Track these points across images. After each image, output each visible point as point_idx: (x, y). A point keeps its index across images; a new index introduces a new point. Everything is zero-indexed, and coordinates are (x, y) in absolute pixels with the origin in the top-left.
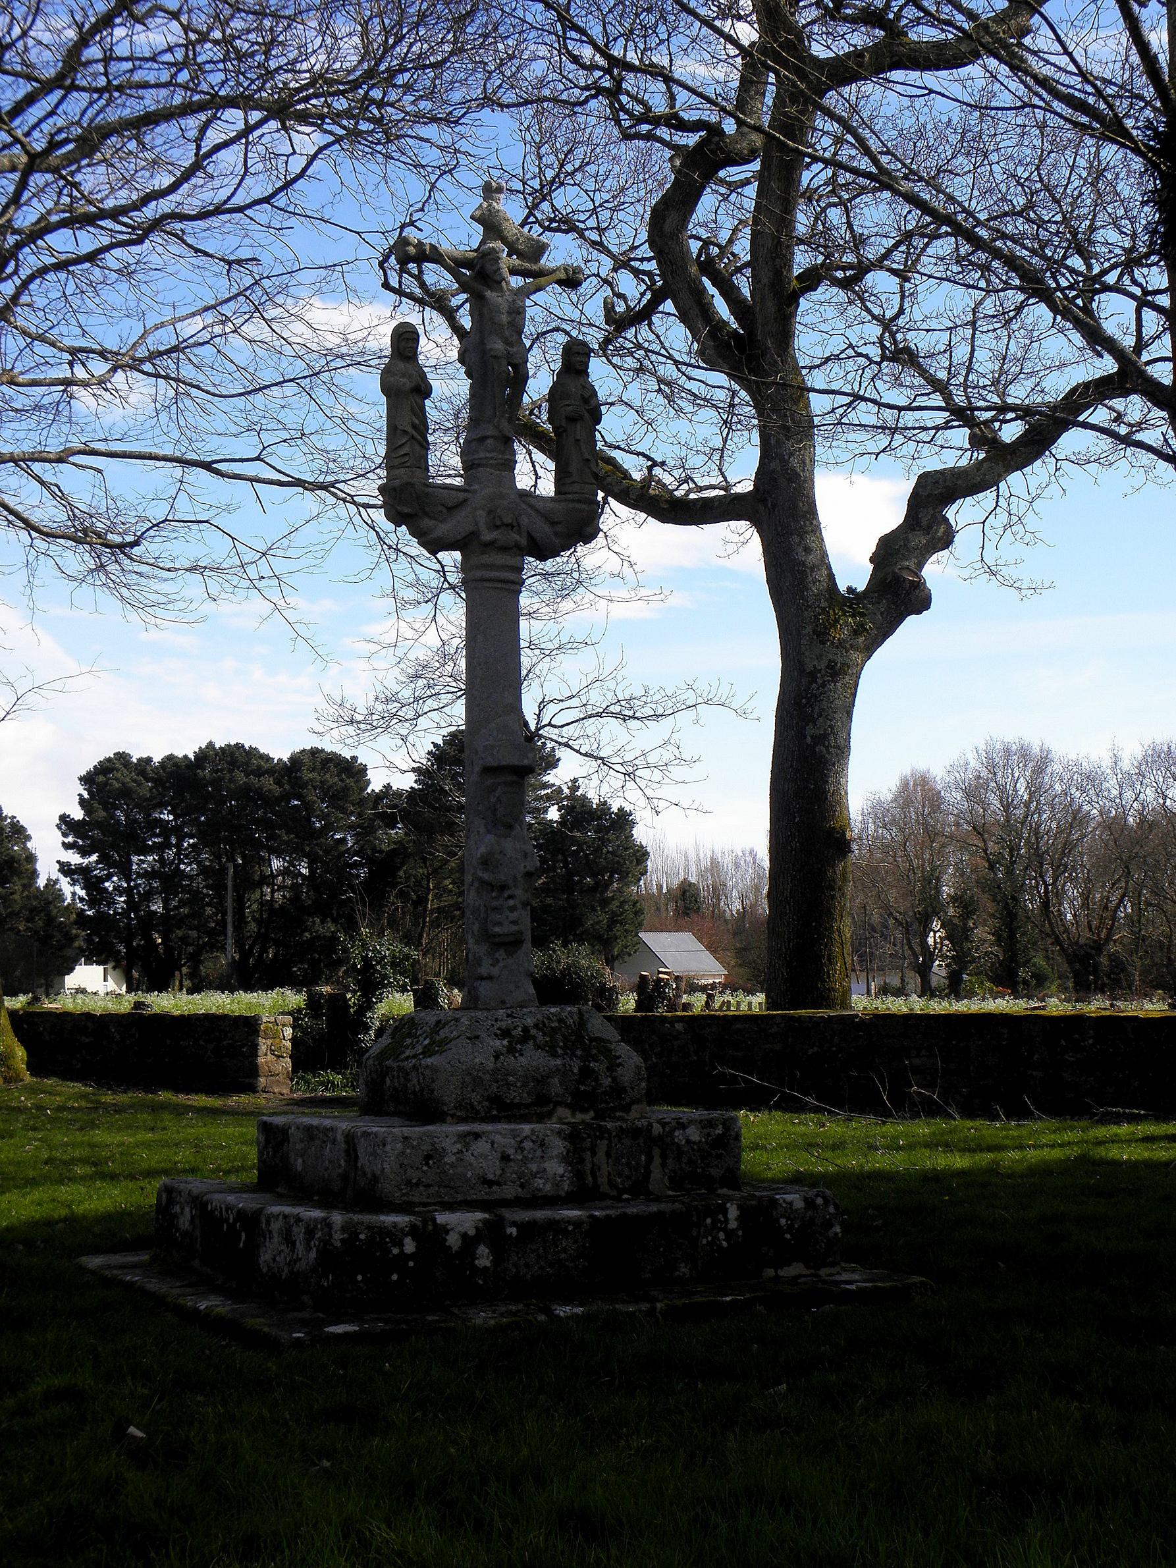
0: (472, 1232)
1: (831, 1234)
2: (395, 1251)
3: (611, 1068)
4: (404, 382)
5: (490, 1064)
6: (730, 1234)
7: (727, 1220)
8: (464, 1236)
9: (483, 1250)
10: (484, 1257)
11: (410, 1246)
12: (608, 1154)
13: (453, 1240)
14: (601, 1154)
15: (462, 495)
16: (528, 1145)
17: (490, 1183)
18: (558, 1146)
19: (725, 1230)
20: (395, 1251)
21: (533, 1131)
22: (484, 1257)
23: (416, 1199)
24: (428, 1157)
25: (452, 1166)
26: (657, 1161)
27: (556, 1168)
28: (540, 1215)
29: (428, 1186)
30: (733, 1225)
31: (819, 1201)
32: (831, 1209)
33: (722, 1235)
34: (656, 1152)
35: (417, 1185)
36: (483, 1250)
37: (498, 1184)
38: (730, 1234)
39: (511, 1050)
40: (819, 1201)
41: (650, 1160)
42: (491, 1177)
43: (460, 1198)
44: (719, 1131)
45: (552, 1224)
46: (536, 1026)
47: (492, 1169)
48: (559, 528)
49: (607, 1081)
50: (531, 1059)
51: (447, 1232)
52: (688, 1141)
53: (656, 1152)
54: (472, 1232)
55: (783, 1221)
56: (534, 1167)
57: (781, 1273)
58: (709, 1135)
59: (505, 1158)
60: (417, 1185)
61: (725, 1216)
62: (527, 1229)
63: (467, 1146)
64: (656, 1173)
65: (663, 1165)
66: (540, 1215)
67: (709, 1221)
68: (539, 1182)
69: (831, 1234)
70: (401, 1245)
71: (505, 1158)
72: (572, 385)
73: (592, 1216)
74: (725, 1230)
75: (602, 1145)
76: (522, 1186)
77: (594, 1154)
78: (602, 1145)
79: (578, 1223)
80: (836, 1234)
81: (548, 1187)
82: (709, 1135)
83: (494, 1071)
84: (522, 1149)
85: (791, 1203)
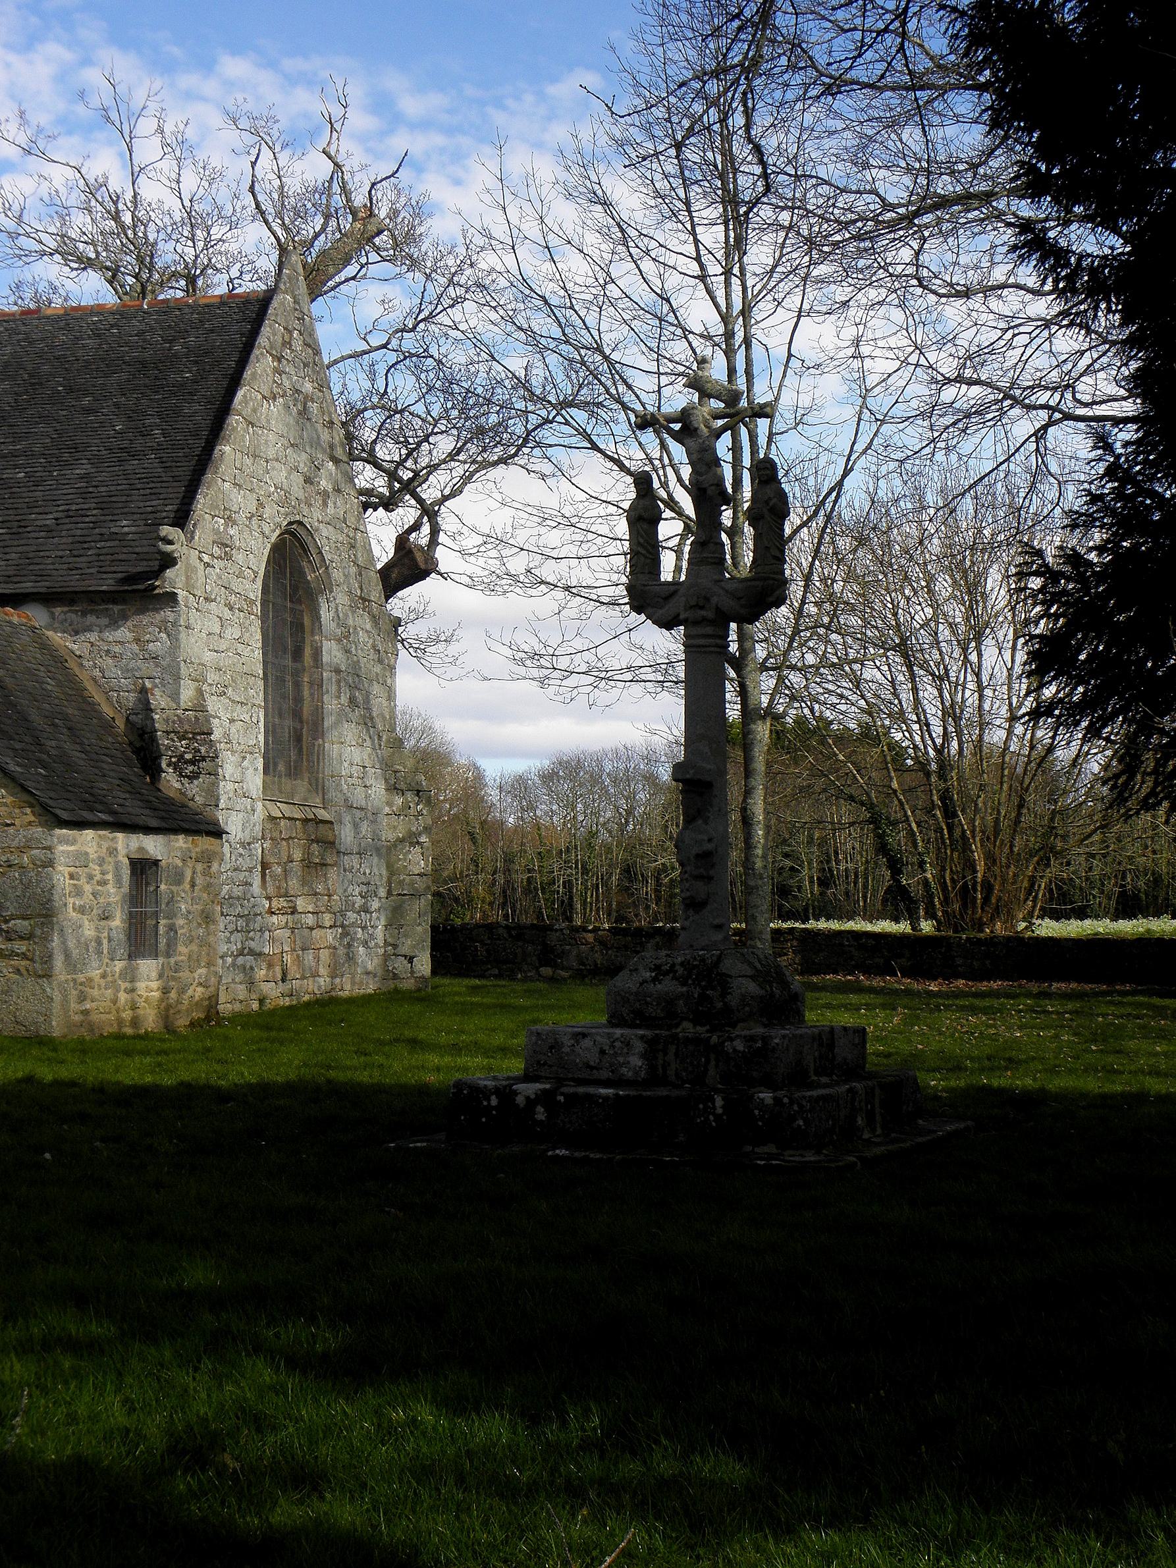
0: (533, 1097)
1: (795, 1125)
2: (485, 1103)
3: (724, 994)
4: (644, 516)
5: (634, 989)
6: (718, 1118)
7: (714, 1108)
8: (528, 1098)
9: (540, 1109)
10: (540, 1113)
11: (494, 1101)
12: (676, 1055)
13: (520, 1100)
14: (671, 1056)
15: (672, 588)
16: (617, 1044)
17: (592, 1068)
18: (639, 1046)
19: (714, 1114)
20: (485, 1103)
21: (622, 1035)
22: (540, 1113)
23: (543, 1074)
24: (551, 1048)
25: (567, 1054)
26: (713, 1063)
27: (636, 1061)
28: (581, 1090)
29: (551, 1066)
30: (720, 1111)
31: (786, 1100)
32: (796, 1107)
33: (711, 1118)
34: (712, 1056)
35: (544, 1064)
36: (540, 1109)
37: (597, 1069)
38: (718, 1118)
39: (655, 980)
40: (786, 1100)
41: (708, 1061)
42: (592, 1063)
43: (570, 1076)
44: (759, 1045)
45: (588, 1096)
46: (682, 964)
47: (593, 1058)
48: (743, 602)
49: (720, 1005)
50: (668, 986)
51: (517, 1094)
52: (735, 1050)
53: (712, 1056)
54: (533, 1097)
55: (756, 1112)
56: (621, 1059)
57: (757, 1150)
58: (750, 1047)
59: (602, 1052)
60: (544, 1064)
61: (713, 1103)
62: (572, 1099)
63: (578, 1042)
64: (712, 1072)
65: (717, 1066)
66: (581, 1090)
67: (701, 1106)
68: (624, 1070)
69: (795, 1125)
70: (489, 1100)
71: (602, 1052)
72: (769, 491)
73: (617, 1095)
74: (714, 1114)
75: (672, 1049)
76: (612, 1071)
77: (666, 1054)
78: (672, 1049)
79: (606, 1098)
80: (799, 1126)
81: (630, 1074)
82: (750, 1047)
83: (637, 994)
84: (614, 1047)
85: (763, 1100)
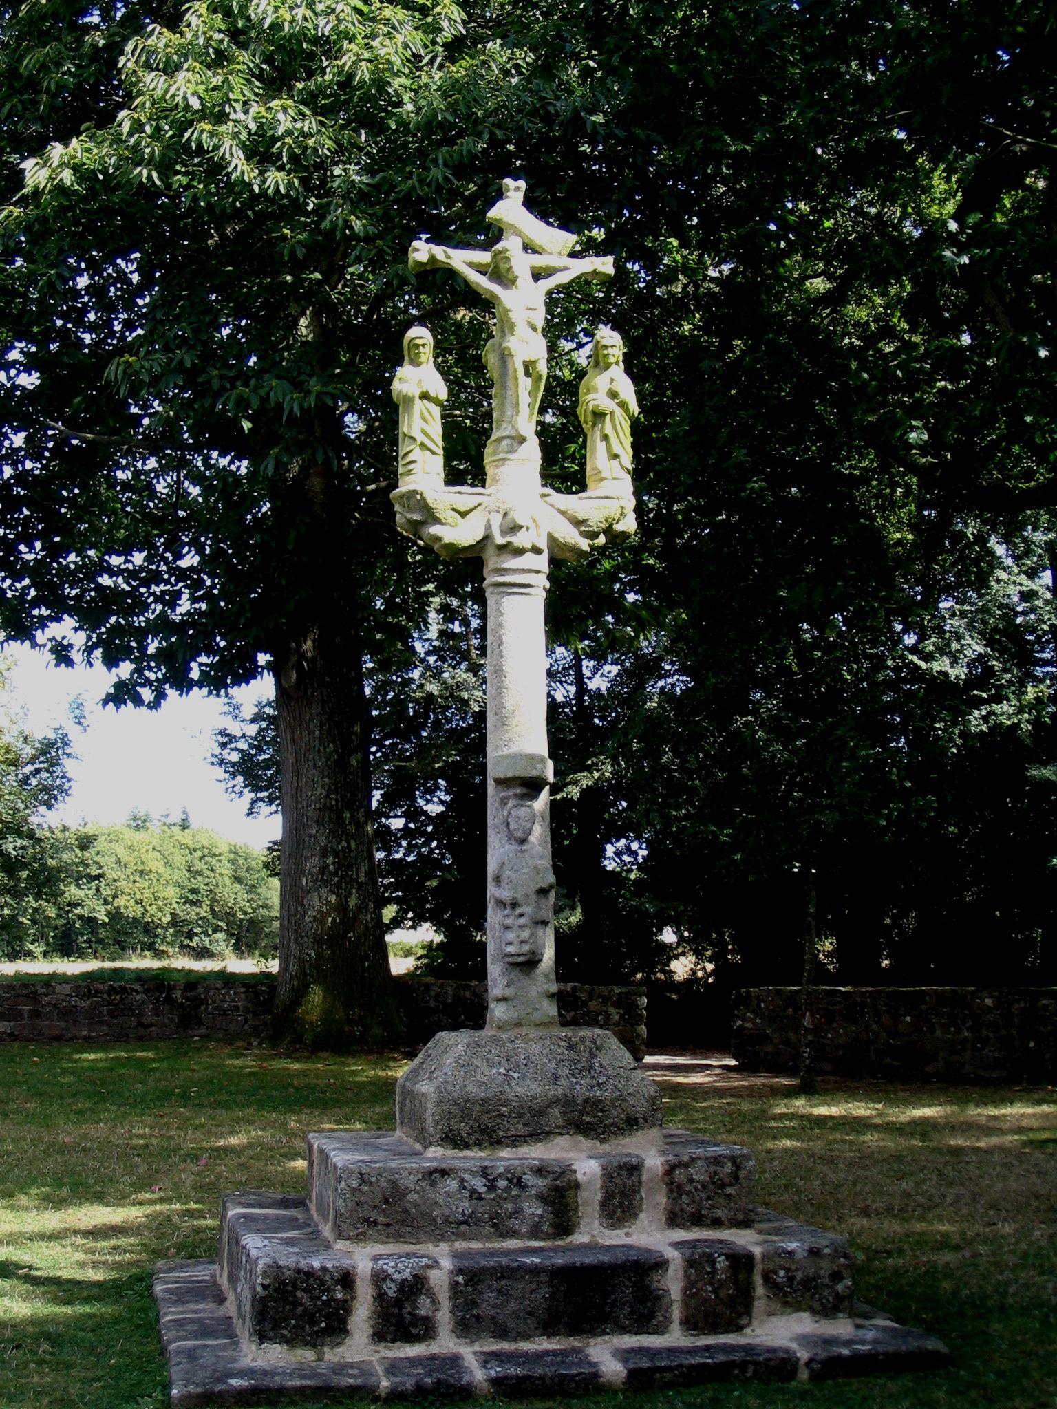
63: (433, 1184)
